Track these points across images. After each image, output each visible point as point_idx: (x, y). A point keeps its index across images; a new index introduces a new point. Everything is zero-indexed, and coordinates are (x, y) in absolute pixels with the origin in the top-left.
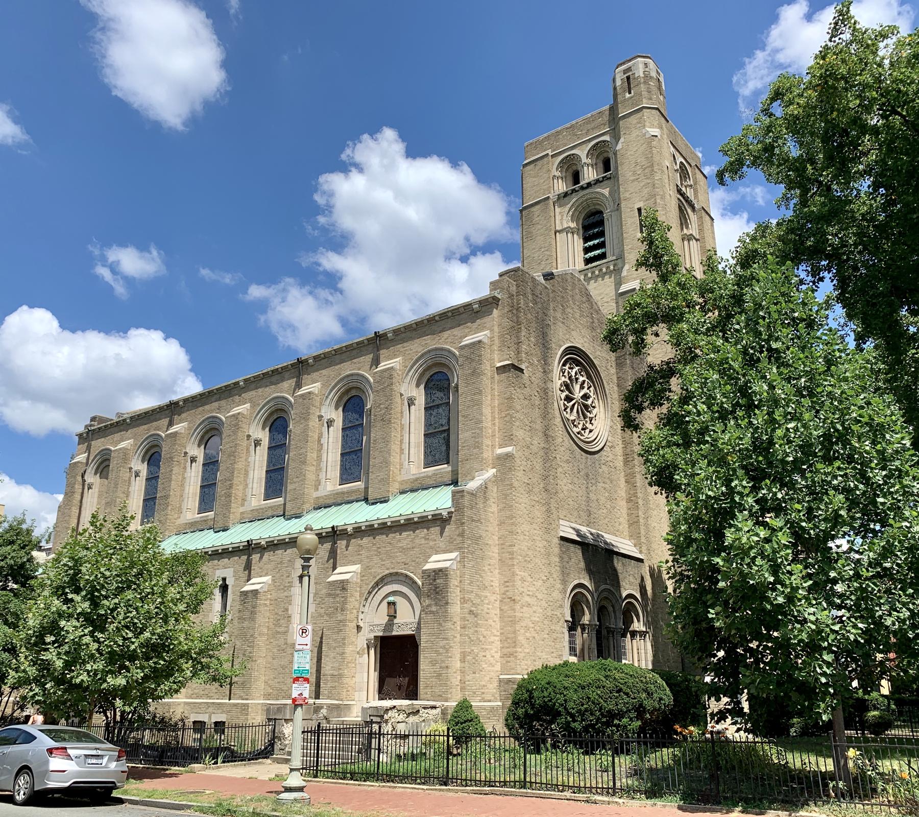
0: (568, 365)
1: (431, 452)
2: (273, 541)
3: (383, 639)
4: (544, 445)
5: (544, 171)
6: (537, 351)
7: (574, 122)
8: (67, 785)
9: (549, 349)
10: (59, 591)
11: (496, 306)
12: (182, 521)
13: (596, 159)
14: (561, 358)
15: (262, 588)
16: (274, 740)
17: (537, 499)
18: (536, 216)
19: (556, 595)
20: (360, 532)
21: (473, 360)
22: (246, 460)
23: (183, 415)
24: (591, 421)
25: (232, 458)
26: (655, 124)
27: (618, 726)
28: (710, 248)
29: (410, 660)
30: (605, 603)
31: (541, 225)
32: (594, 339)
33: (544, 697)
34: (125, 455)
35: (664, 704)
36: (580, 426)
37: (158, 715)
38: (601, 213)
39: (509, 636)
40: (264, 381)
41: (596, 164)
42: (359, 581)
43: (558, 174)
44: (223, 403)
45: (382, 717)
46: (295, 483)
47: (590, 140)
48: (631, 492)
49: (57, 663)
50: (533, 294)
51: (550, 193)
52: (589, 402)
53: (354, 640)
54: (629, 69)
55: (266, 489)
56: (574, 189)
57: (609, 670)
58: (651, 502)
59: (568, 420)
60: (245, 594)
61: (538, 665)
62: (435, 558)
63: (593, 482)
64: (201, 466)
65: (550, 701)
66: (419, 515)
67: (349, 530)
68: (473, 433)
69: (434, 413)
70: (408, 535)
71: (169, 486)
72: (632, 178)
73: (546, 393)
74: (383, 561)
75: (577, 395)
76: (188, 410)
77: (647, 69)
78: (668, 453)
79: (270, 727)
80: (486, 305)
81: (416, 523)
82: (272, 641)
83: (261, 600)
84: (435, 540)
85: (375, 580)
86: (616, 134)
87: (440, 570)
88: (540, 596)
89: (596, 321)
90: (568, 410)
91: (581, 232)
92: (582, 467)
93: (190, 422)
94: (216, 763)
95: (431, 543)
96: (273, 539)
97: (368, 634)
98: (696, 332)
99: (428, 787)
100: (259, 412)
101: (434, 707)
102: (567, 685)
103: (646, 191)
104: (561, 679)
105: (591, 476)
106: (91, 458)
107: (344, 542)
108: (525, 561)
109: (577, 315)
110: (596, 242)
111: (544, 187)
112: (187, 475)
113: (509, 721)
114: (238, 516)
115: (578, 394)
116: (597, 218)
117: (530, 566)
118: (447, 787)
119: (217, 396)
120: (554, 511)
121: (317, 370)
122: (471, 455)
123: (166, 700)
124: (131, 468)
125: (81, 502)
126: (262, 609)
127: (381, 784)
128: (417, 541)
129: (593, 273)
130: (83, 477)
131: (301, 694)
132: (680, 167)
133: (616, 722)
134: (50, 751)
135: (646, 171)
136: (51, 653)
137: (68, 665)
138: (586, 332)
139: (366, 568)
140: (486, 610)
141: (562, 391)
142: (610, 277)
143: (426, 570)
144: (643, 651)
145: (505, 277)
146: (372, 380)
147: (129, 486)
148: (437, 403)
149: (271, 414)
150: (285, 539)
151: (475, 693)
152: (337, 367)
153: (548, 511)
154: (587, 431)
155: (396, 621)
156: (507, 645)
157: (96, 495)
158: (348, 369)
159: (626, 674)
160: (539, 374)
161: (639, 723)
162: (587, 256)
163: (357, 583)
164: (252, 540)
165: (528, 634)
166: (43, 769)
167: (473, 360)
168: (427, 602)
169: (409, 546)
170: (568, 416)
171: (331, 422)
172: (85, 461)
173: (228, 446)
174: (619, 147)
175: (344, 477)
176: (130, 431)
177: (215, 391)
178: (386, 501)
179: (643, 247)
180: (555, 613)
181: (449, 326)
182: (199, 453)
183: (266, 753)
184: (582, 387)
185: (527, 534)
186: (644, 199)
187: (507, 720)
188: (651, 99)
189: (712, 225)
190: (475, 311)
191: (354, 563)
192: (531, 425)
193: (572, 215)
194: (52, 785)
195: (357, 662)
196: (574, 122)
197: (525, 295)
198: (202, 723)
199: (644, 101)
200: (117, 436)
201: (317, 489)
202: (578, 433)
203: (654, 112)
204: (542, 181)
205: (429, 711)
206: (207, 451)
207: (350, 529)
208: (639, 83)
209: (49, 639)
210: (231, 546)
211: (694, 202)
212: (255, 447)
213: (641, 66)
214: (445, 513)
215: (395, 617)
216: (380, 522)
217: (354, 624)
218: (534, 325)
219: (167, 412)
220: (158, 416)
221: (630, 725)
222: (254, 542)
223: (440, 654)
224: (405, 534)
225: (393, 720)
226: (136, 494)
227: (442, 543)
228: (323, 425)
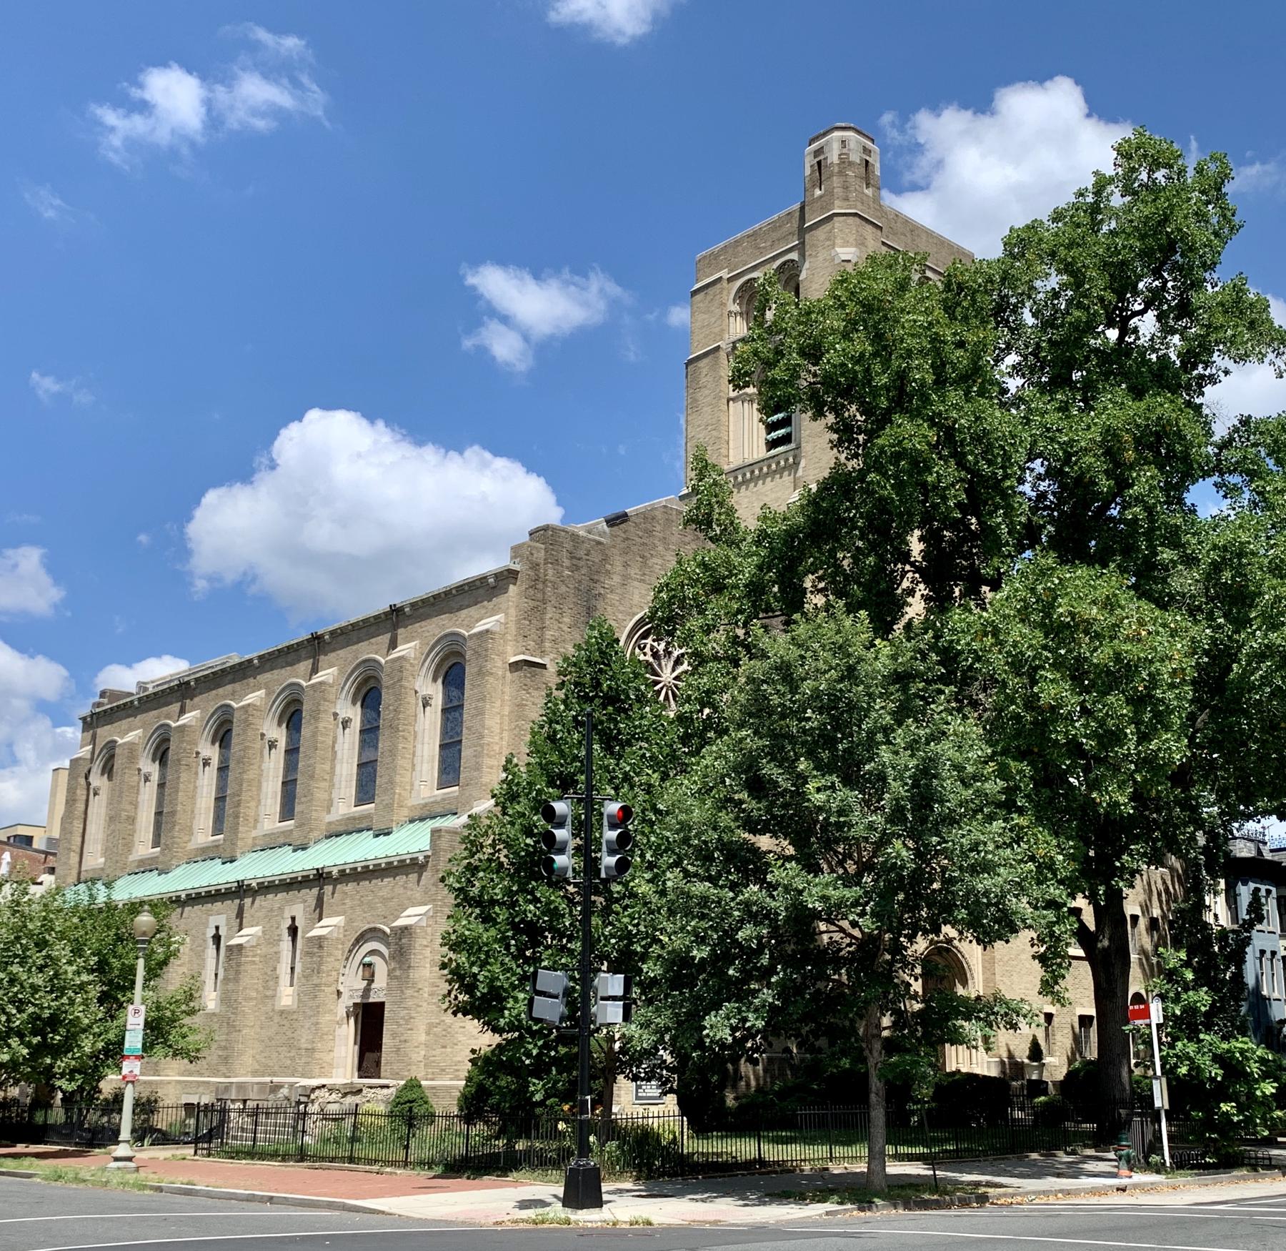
5: (716, 303)
7: (757, 226)
11: (513, 581)
12: (191, 846)
15: (248, 941)
20: (267, 888)
22: (260, 767)
25: (241, 765)
26: (851, 240)
34: (131, 748)
40: (280, 660)
42: (341, 936)
43: (736, 308)
44: (237, 686)
45: (308, 1096)
47: (774, 258)
51: (721, 339)
53: (332, 1007)
62: (410, 911)
64: (215, 771)
70: (389, 882)
71: (176, 799)
76: (201, 694)
77: (845, 151)
83: (247, 956)
97: (348, 1001)
100: (274, 702)
101: (388, 1087)
106: (97, 753)
107: (330, 888)
112: (199, 783)
114: (250, 841)
121: (334, 650)
124: (139, 770)
125: (86, 813)
126: (249, 967)
130: (87, 777)
131: (131, 1072)
139: (350, 921)
142: (790, 475)
147: (138, 793)
151: (444, 1070)
152: (355, 647)
155: (373, 986)
157: (104, 804)
163: (338, 939)
171: (347, 722)
176: (139, 717)
178: (388, 834)
181: (467, 603)
188: (847, 199)
196: (757, 226)
197: (556, 562)
199: (837, 203)
200: (124, 724)
201: (329, 812)
203: (851, 220)
207: (335, 871)
208: (831, 176)
212: (270, 750)
213: (836, 147)
215: (373, 981)
217: (333, 989)
225: (321, 1100)
226: (146, 804)
227: (417, 893)
228: (338, 727)
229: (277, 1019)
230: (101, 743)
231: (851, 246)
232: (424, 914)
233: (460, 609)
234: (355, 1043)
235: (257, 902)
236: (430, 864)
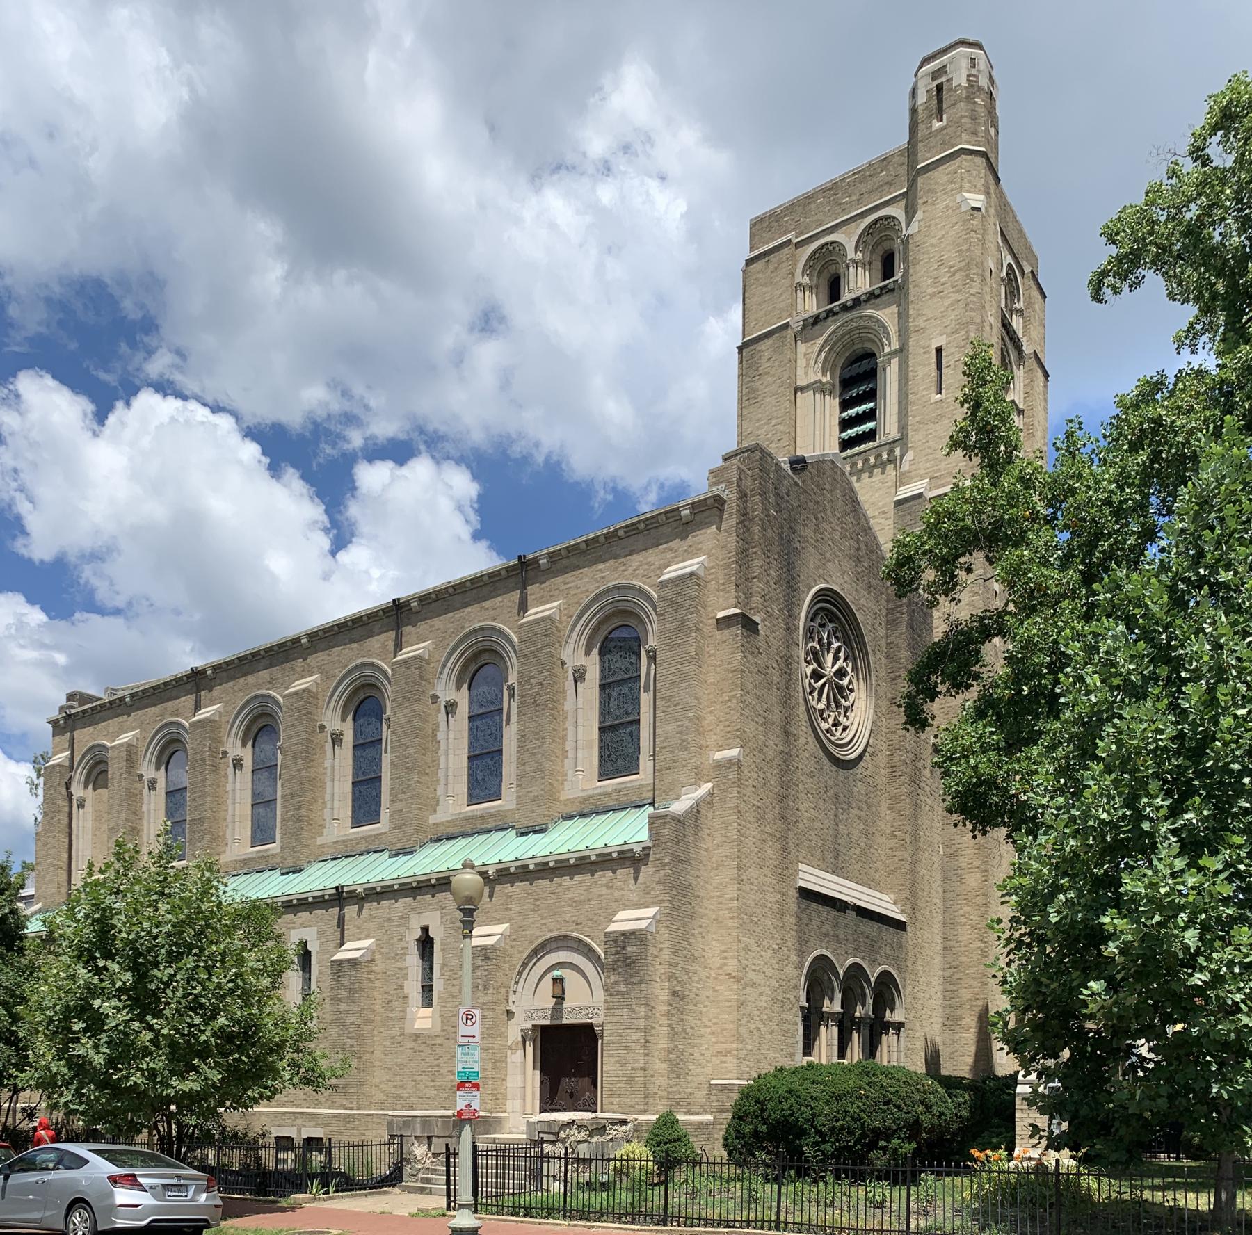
0: (818, 620)
1: (609, 756)
2: (374, 888)
3: (544, 1028)
4: (782, 748)
6: (778, 593)
8: (145, 1223)
9: (795, 590)
10: (85, 956)
13: (818, 277)
14: (810, 607)
16: (401, 1162)
17: (770, 831)
18: (764, 359)
19: (790, 971)
20: (377, 894)
21: (680, 607)
23: (217, 690)
24: (846, 712)
27: (884, 1149)
28: (1073, 417)
29: (584, 1058)
32: (858, 577)
33: (783, 1110)
35: (946, 1120)
36: (831, 720)
37: (228, 1129)
38: (872, 355)
39: (726, 1026)
41: (870, 263)
45: (557, 1134)
46: (401, 801)
48: (895, 824)
49: (96, 1057)
50: (777, 494)
52: (845, 682)
54: (942, 70)
55: (354, 811)
56: (831, 311)
57: (874, 1075)
58: (922, 840)
60: (339, 963)
61: (766, 1068)
62: (621, 915)
63: (845, 807)
64: (250, 774)
65: (792, 1115)
66: (598, 852)
67: (490, 872)
68: (678, 726)
69: (615, 694)
70: (581, 882)
72: (931, 290)
73: (788, 664)
74: (543, 918)
75: (828, 669)
78: (984, 764)
79: (396, 1146)
80: (709, 509)
81: (592, 863)
82: (382, 1030)
84: (623, 889)
85: (533, 947)
86: (910, 202)
87: (633, 933)
88: (769, 972)
89: (863, 547)
90: (816, 694)
91: (837, 390)
92: (831, 783)
93: (226, 703)
94: (327, 1192)
95: (617, 894)
96: (374, 885)
98: (1045, 563)
99: (638, 1227)
100: (336, 688)
101: (624, 1122)
102: (815, 1095)
103: (952, 316)
104: (805, 1086)
105: (842, 798)
108: (752, 922)
109: (837, 536)
110: (861, 409)
111: (782, 305)
113: (730, 1141)
115: (830, 669)
116: (865, 366)
117: (758, 930)
118: (667, 1228)
119: (266, 662)
120: (792, 848)
122: (674, 761)
123: (255, 1109)
127: (572, 1223)
128: (595, 890)
132: (1007, 274)
133: (883, 1143)
134: (114, 1180)
135: (957, 276)
136: (83, 1044)
137: (111, 1062)
138: (847, 565)
139: (518, 929)
140: (694, 991)
141: (808, 662)
143: (611, 933)
144: (895, 1049)
145: (735, 461)
146: (515, 639)
148: (620, 677)
149: (355, 692)
150: (393, 886)
151: (678, 1103)
153: (785, 849)
154: (840, 728)
156: (722, 1040)
158: (475, 617)
159: (898, 1080)
160: (780, 633)
161: (914, 1145)
162: (844, 435)
164: (342, 887)
165: (752, 1026)
166: (108, 1202)
167: (680, 607)
168: (613, 978)
169: (582, 898)
170: (814, 703)
172: (67, 764)
173: (290, 742)
174: (914, 227)
175: (476, 792)
177: (262, 653)
178: (411, 853)
179: (962, 412)
182: (247, 754)
183: (393, 1179)
184: (836, 659)
185: (756, 882)
186: (949, 330)
187: (725, 1139)
188: (975, 133)
189: (1045, 386)
190: (684, 520)
191: (500, 922)
192: (766, 714)
193: (825, 359)
194: (121, 1223)
195: (509, 1060)
198: (290, 1139)
200: (113, 724)
205: (618, 1127)
206: (474, 692)
209: (78, 1026)
210: (310, 894)
211: (1024, 340)
213: (965, 63)
214: (638, 849)
215: (563, 999)
216: (537, 861)
217: (503, 1008)
218: (775, 548)
219: (188, 686)
220: (174, 693)
221: (901, 1148)
222: (346, 889)
223: (633, 1050)
224: (578, 878)
229: (409, 1044)
230: (80, 750)
231: (978, 192)
232: (653, 918)
233: (631, 553)
234: (534, 1068)
235: (365, 910)
236: (651, 858)
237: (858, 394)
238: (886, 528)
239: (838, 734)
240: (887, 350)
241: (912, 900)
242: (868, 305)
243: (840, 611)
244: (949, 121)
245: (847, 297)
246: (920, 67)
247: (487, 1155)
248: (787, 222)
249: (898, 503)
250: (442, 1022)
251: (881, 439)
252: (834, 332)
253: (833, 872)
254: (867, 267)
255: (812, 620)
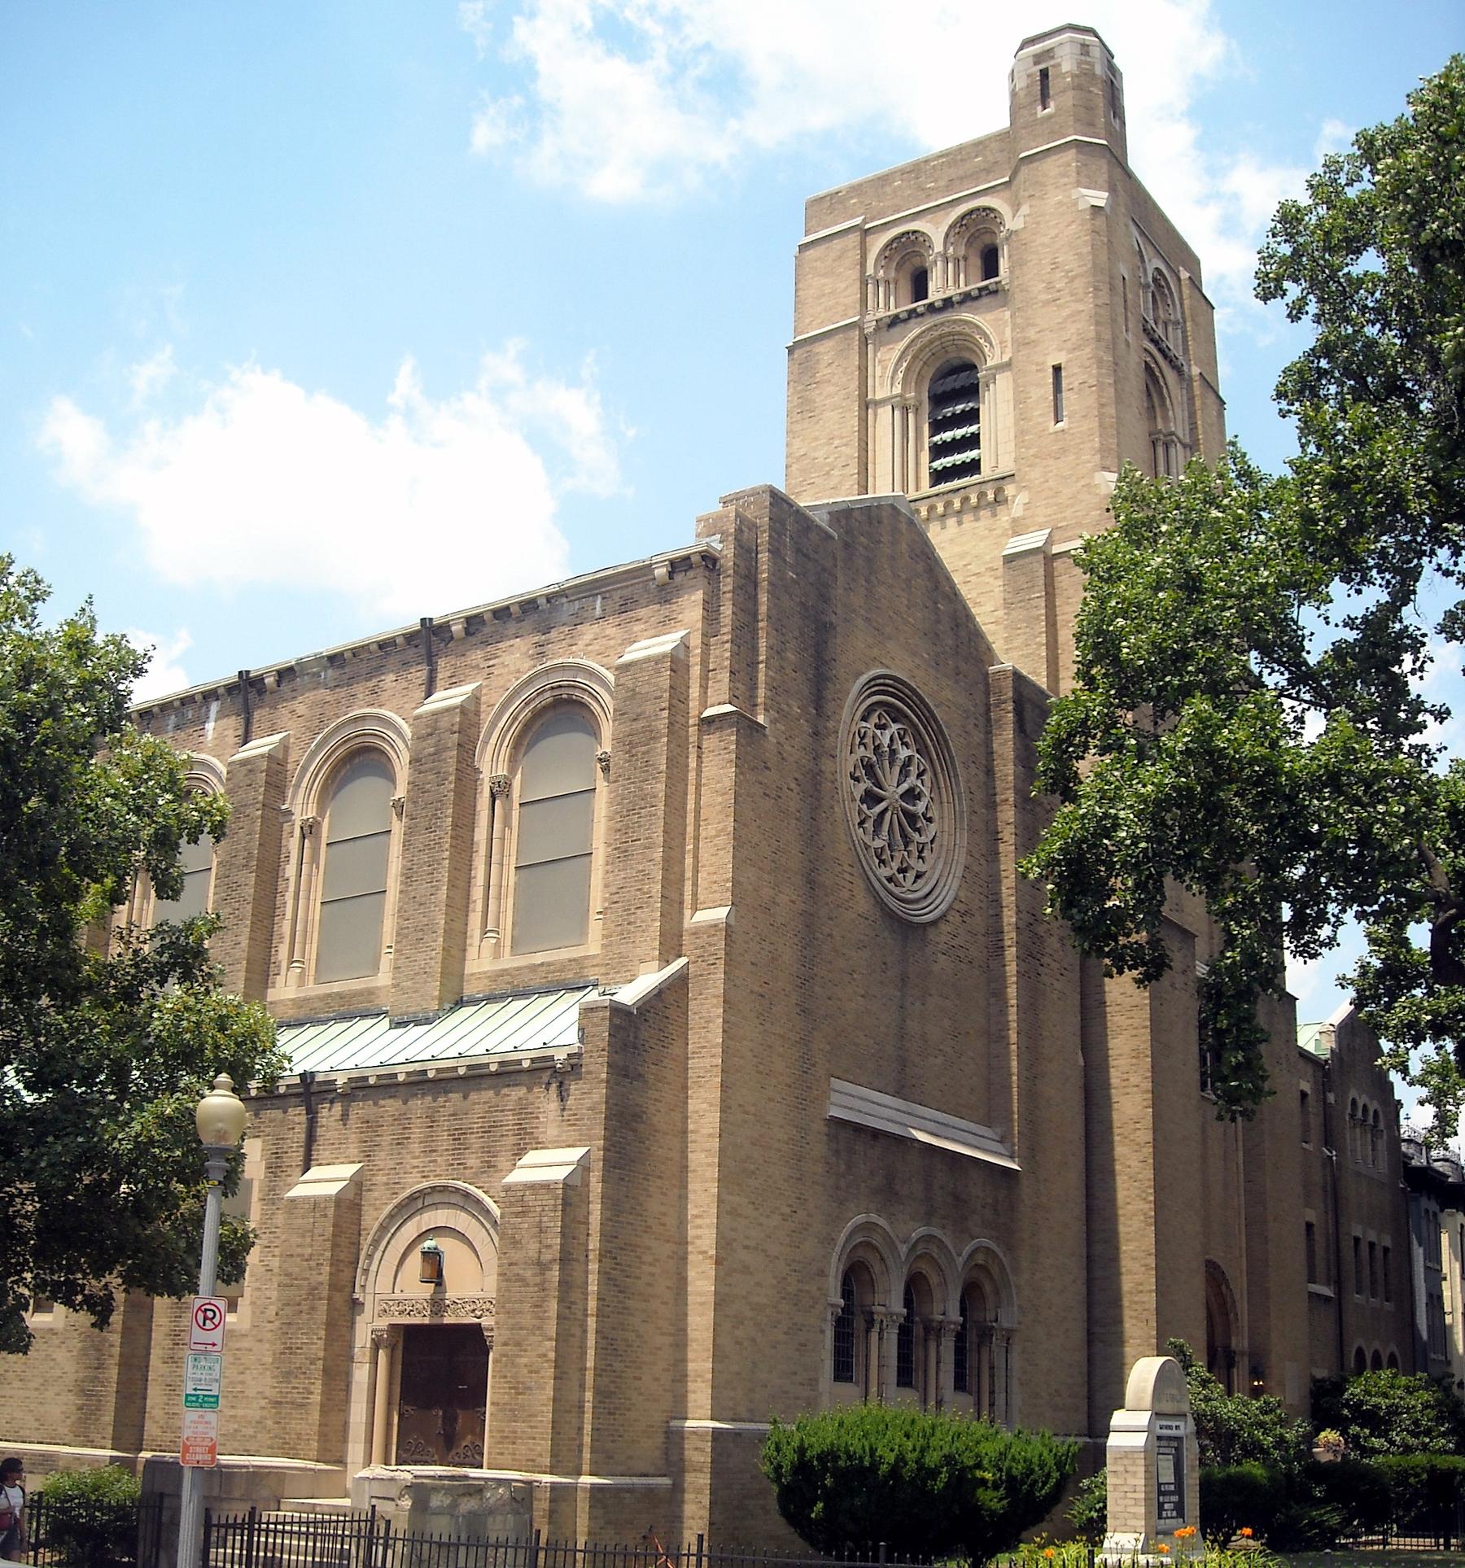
0: (874, 719)
24: (920, 852)
30: (925, 1268)
31: (836, 385)
36: (895, 865)
38: (972, 367)
52: (920, 807)
54: (1048, 54)
59: (867, 847)
67: (340, 1082)
72: (1044, 297)
90: (869, 825)
107: (338, 1108)
110: (959, 433)
115: (893, 789)
129: (949, 504)
132: (1155, 280)
141: (857, 780)
154: (911, 875)
180: (807, 1288)
186: (1069, 345)
193: (908, 369)
202: (890, 880)
204: (843, 285)
207: (341, 1080)
214: (561, 1056)
237: (954, 414)
238: (997, 590)
239: (908, 884)
240: (990, 363)
241: (1031, 1152)
242: (963, 308)
243: (909, 707)
244: (1058, 109)
245: (935, 293)
246: (1021, 48)
247: (276, 1531)
248: (855, 204)
249: (1009, 559)
250: (253, 1312)
251: (986, 471)
252: (918, 337)
253: (897, 1094)
254: (962, 263)
255: (864, 719)
